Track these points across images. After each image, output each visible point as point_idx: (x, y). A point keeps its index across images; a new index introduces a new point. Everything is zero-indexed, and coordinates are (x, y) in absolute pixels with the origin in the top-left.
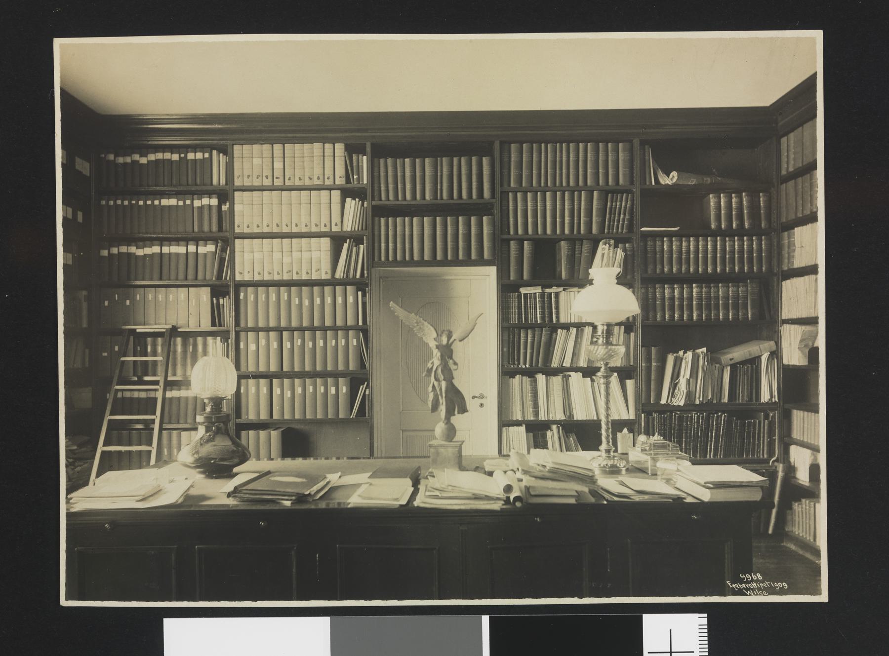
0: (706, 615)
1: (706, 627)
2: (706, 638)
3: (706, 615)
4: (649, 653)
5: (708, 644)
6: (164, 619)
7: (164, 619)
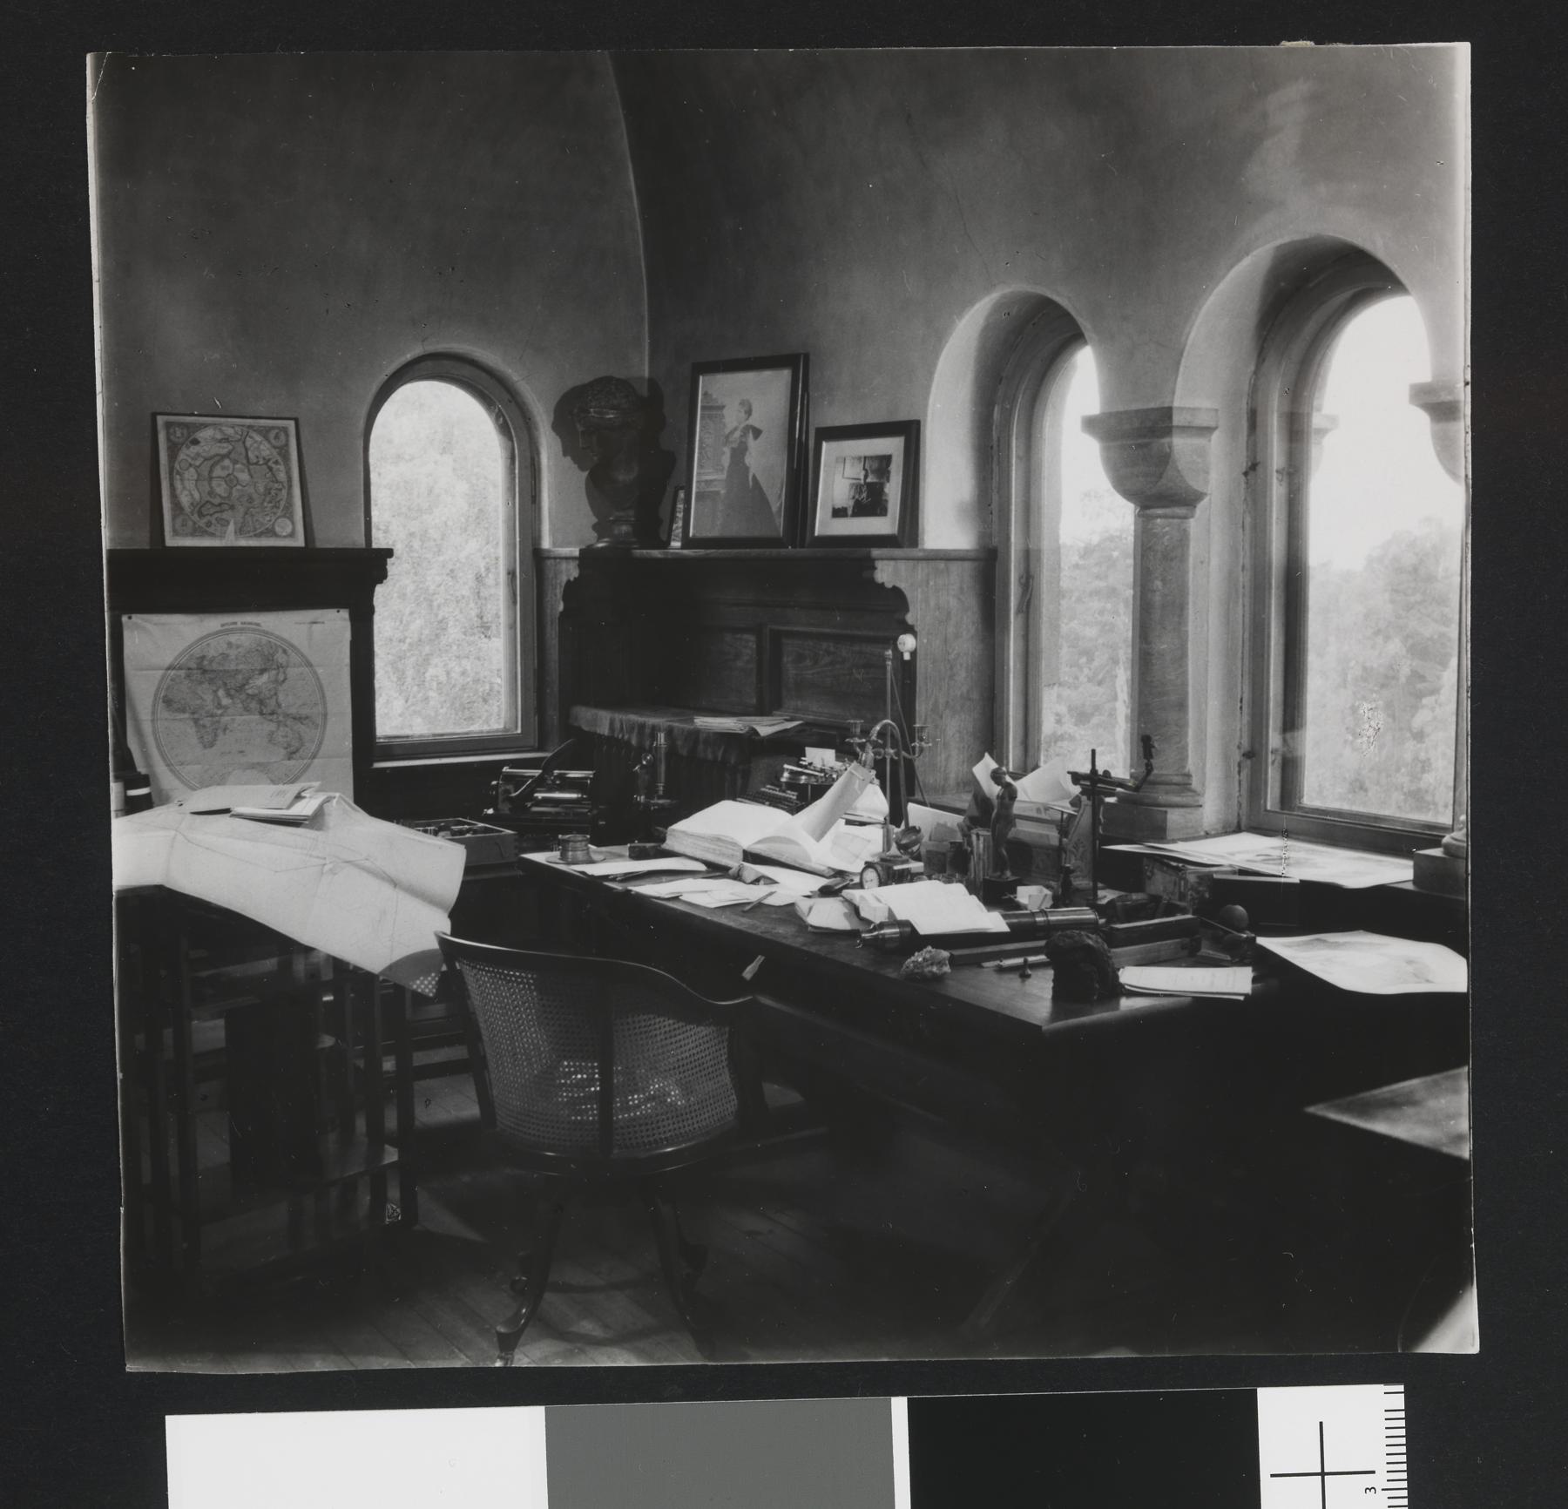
0: (1401, 1388)
1: (1402, 1414)
2: (1405, 1493)
3: (1401, 1388)
4: (1272, 1476)
5: (1408, 1462)
6: (166, 1417)
7: (166, 1417)
